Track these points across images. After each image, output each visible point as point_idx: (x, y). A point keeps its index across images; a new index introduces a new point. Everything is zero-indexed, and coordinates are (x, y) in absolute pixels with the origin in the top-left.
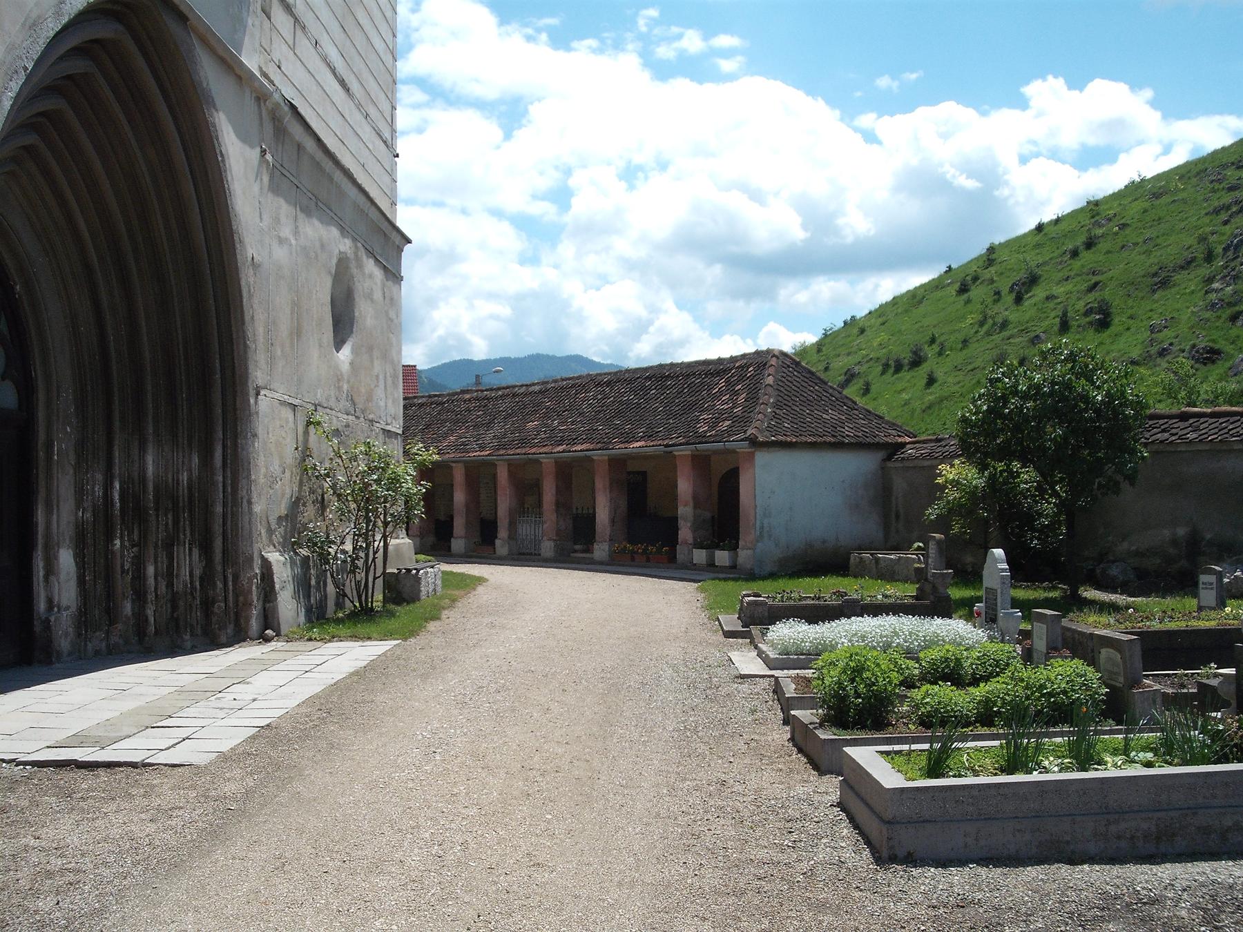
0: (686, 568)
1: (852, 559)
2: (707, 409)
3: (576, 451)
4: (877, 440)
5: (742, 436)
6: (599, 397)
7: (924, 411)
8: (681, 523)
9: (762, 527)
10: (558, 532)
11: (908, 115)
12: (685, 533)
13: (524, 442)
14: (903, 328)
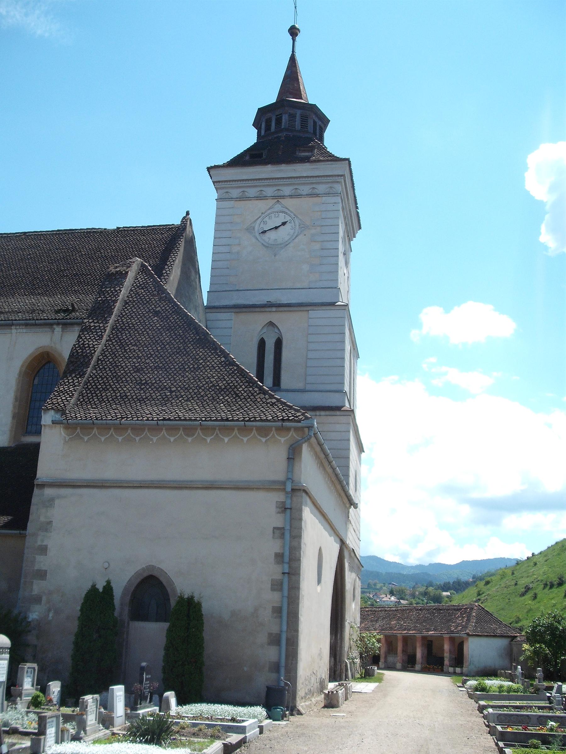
0: (447, 673)
1: (498, 672)
2: (454, 622)
3: (410, 633)
4: (508, 635)
5: (465, 632)
6: (418, 614)
7: (562, 610)
8: (445, 659)
9: (471, 661)
10: (403, 660)
11: (503, 557)
12: (446, 662)
13: (391, 628)
14: (556, 564)
